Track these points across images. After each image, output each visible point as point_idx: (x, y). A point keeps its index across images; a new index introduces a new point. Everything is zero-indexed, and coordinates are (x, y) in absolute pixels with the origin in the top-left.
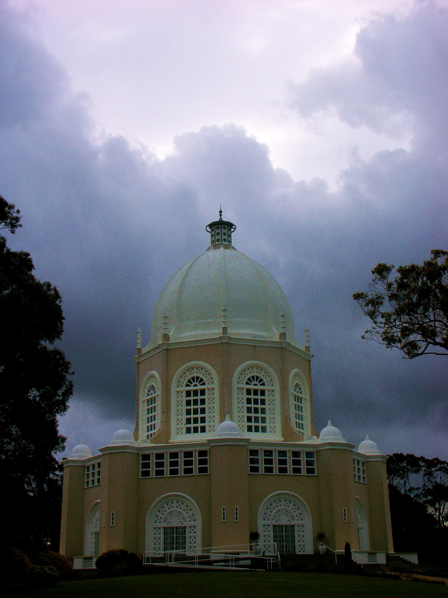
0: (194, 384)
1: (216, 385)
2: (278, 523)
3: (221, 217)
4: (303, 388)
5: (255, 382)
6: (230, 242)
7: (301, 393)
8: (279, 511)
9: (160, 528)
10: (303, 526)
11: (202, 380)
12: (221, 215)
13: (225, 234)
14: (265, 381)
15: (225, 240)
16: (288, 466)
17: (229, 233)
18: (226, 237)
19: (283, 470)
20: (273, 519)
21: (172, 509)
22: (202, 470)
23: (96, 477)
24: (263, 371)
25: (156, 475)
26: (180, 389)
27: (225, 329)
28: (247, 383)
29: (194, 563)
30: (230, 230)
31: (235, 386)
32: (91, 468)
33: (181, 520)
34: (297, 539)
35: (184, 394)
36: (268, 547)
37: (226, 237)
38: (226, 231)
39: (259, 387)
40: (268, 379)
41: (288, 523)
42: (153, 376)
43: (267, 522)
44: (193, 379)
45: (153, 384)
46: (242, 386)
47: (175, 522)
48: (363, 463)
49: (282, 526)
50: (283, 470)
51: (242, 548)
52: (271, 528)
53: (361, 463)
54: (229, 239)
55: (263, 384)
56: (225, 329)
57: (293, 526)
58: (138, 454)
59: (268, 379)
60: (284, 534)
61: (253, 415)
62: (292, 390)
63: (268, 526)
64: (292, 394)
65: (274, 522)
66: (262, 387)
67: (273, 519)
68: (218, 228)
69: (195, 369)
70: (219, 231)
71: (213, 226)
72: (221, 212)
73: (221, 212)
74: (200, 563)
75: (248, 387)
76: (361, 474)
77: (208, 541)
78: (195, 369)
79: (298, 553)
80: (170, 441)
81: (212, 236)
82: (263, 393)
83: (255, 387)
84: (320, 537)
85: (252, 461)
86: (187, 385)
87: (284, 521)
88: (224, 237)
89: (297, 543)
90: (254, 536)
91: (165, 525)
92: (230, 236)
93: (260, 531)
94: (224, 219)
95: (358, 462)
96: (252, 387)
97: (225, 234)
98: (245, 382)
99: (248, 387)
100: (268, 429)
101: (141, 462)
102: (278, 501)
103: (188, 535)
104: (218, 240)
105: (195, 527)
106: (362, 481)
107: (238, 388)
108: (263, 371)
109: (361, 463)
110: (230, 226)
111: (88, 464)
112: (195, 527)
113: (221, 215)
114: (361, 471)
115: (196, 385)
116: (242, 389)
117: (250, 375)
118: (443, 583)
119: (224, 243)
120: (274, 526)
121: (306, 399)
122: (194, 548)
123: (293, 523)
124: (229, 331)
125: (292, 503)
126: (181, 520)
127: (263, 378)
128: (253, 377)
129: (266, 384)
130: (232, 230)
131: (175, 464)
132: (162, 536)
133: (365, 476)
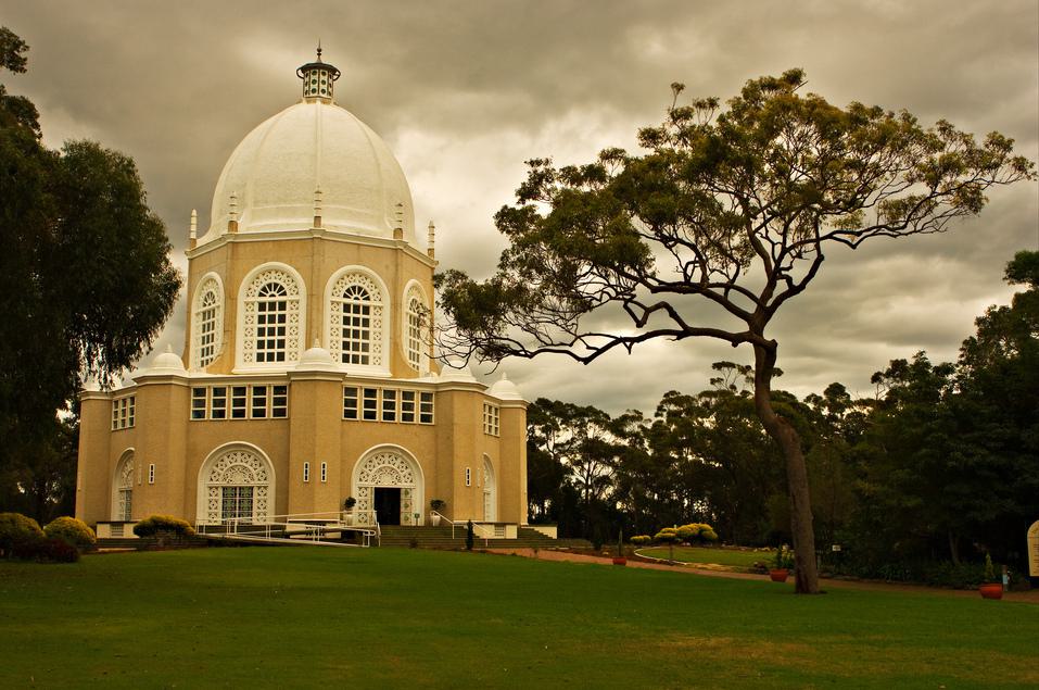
0: (270, 293)
1: (302, 297)
5: (356, 295)
8: (381, 469)
11: (282, 288)
13: (324, 82)
14: (370, 294)
15: (323, 91)
16: (377, 410)
20: (373, 480)
22: (425, 418)
24: (369, 280)
25: (234, 416)
27: (317, 218)
28: (345, 296)
29: (264, 535)
32: (129, 401)
33: (247, 478)
35: (256, 307)
39: (362, 302)
41: (245, 484)
42: (212, 280)
47: (238, 480)
51: (327, 511)
52: (220, 491)
55: (368, 299)
56: (317, 218)
61: (351, 340)
66: (366, 303)
75: (347, 301)
77: (283, 505)
82: (366, 310)
83: (272, 299)
84: (437, 505)
85: (347, 403)
91: (225, 484)
93: (355, 496)
96: (267, 299)
97: (324, 82)
98: (257, 293)
99: (347, 301)
100: (371, 360)
103: (255, 498)
107: (333, 303)
111: (116, 398)
116: (338, 303)
117: (265, 283)
119: (321, 94)
120: (224, 488)
122: (264, 514)
124: (323, 221)
125: (399, 460)
126: (247, 478)
128: (354, 288)
132: (220, 498)
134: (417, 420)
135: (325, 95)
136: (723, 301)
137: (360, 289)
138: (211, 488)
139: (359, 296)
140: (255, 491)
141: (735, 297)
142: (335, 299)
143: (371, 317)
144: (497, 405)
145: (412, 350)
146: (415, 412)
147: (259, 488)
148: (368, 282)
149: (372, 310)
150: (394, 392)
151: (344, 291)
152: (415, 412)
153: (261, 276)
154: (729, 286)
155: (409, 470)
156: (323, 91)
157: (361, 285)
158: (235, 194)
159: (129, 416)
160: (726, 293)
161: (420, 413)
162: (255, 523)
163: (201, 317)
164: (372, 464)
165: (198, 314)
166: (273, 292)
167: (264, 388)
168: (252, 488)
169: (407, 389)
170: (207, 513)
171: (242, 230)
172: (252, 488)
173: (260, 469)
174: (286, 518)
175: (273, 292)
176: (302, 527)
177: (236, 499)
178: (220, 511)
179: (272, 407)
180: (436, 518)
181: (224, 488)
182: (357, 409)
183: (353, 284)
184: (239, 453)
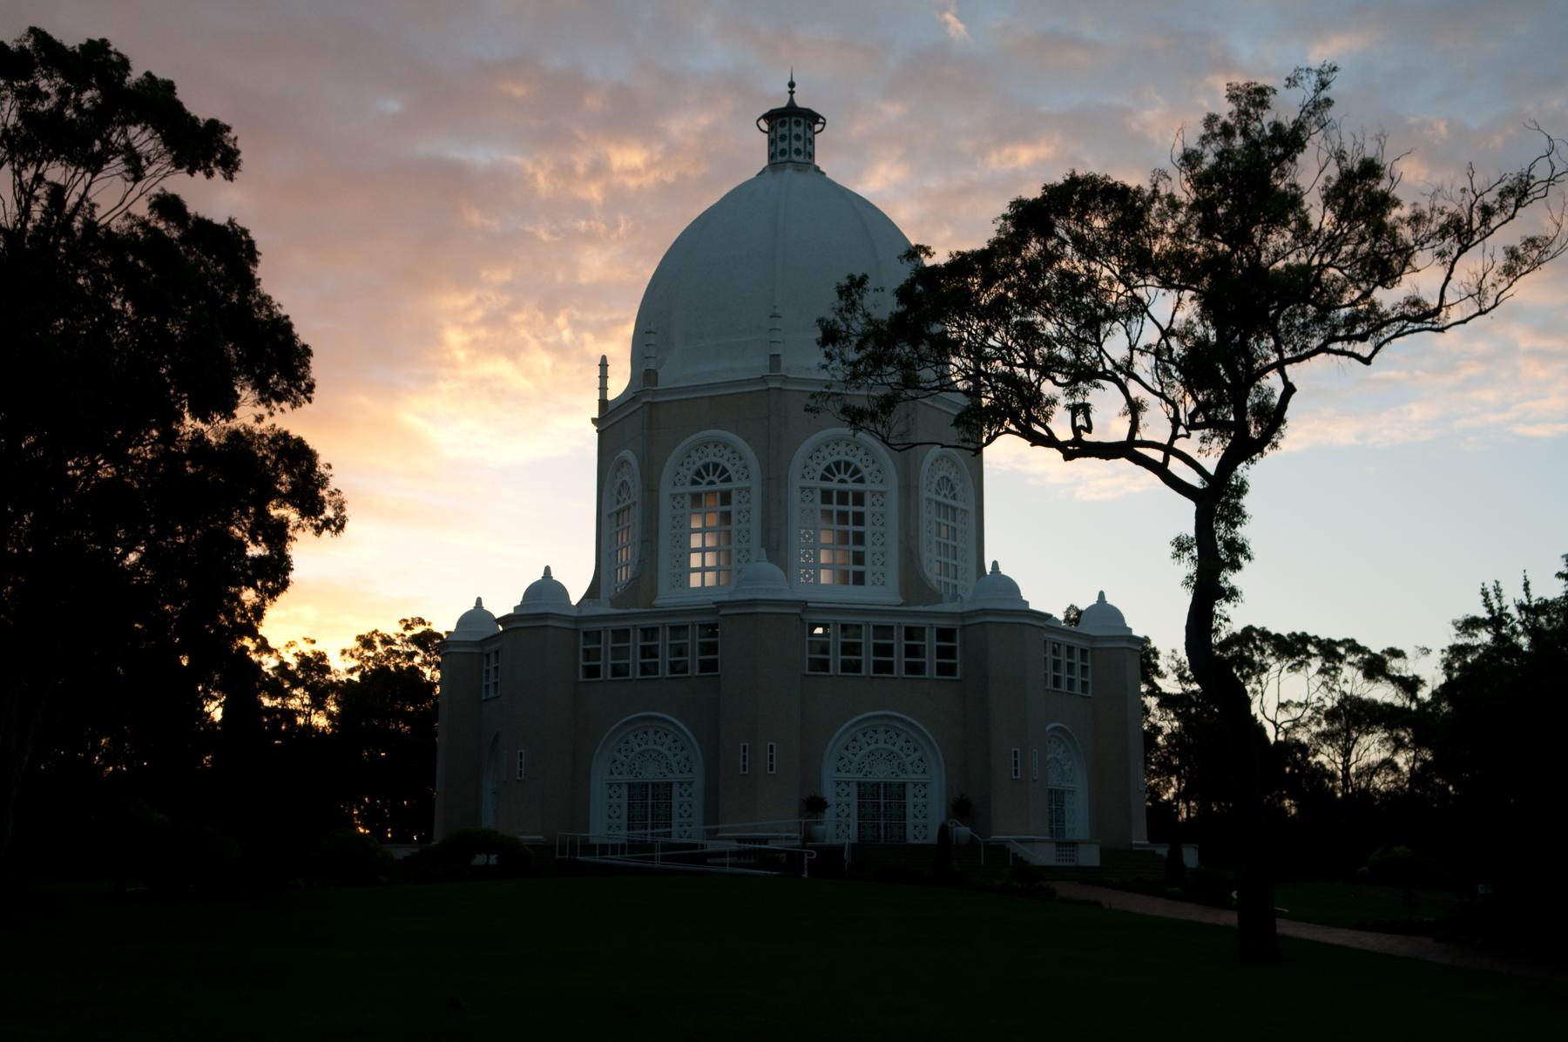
0: (707, 479)
1: (755, 484)
2: (871, 779)
3: (792, 99)
4: (958, 488)
5: (842, 476)
6: (811, 155)
7: (954, 497)
8: (872, 753)
9: (619, 785)
10: (924, 785)
11: (725, 470)
12: (792, 93)
13: (798, 137)
14: (865, 472)
15: (798, 152)
16: (895, 659)
17: (809, 134)
18: (799, 145)
19: (883, 668)
20: (859, 770)
21: (644, 747)
22: (944, 670)
23: (492, 680)
24: (862, 451)
25: (939, 673)
26: (680, 490)
27: (775, 358)
28: (823, 478)
29: (652, 858)
30: (811, 128)
31: (796, 481)
32: (492, 656)
33: (664, 770)
34: (910, 811)
35: (818, 496)
36: (840, 827)
37: (799, 145)
38: (799, 130)
39: (851, 486)
40: (873, 468)
41: (892, 779)
42: (624, 462)
43: (843, 776)
44: (706, 467)
45: (626, 478)
46: (811, 484)
47: (651, 774)
48: (1084, 652)
49: (878, 785)
50: (883, 668)
51: (779, 828)
52: (854, 790)
53: (1077, 653)
54: (809, 148)
55: (861, 480)
56: (775, 358)
57: (904, 785)
58: (576, 630)
59: (873, 468)
60: (882, 801)
62: (927, 492)
63: (848, 784)
64: (930, 500)
65: (859, 777)
66: (859, 487)
67: (859, 770)
68: (783, 124)
69: (711, 446)
70: (785, 130)
71: (773, 117)
72: (792, 85)
73: (792, 85)
74: (664, 859)
75: (826, 485)
76: (1077, 677)
77: (712, 813)
78: (711, 446)
79: (911, 840)
80: (655, 602)
81: (772, 142)
82: (859, 499)
83: (842, 486)
84: (961, 808)
86: (694, 483)
87: (882, 773)
88: (796, 144)
89: (910, 822)
90: (815, 806)
91: (631, 778)
92: (811, 142)
93: (829, 793)
94: (801, 103)
95: (1070, 649)
96: (834, 485)
97: (798, 137)
98: (818, 475)
99: (826, 485)
100: (868, 578)
101: (582, 647)
102: (870, 733)
103: (676, 800)
104: (783, 152)
105: (690, 784)
106: (1078, 690)
107: (803, 489)
108: (862, 451)
109: (1077, 653)
110: (811, 118)
111: (487, 649)
112: (690, 784)
113: (792, 93)
114: (1078, 670)
115: (711, 483)
116: (812, 490)
117: (830, 460)
118: (1098, 904)
119: (794, 157)
120: (859, 784)
121: (966, 512)
122: (687, 826)
123: (902, 778)
124: (786, 362)
125: (903, 737)
126: (664, 770)
127: (861, 466)
128: (837, 464)
129: (867, 478)
130: (818, 127)
131: (912, 651)
133: (1088, 679)
134: (931, 671)
135: (801, 159)
136: (1161, 470)
137: (848, 465)
138: (611, 785)
139: (846, 477)
140: (676, 788)
141: (1176, 467)
142: (807, 483)
143: (867, 509)
144: (1084, 644)
145: (942, 559)
146: (926, 660)
147: (681, 784)
148: (860, 453)
149: (868, 498)
150: (891, 628)
151: (821, 470)
152: (863, 657)
153: (693, 453)
154: (1169, 450)
155: (919, 754)
156: (798, 152)
157: (849, 459)
158: (653, 328)
159: (492, 680)
160: (1166, 459)
161: (904, 659)
162: (675, 839)
163: (614, 519)
164: (857, 745)
165: (610, 516)
166: (711, 478)
167: (627, 631)
168: (670, 785)
169: (912, 622)
170: (606, 822)
171: (665, 382)
172: (670, 785)
173: (915, 756)
174: (717, 831)
175: (711, 478)
176: (734, 846)
177: (649, 801)
178: (624, 821)
179: (698, 657)
180: (963, 831)
181: (859, 784)
182: (831, 657)
183: (836, 458)
184: (651, 731)
